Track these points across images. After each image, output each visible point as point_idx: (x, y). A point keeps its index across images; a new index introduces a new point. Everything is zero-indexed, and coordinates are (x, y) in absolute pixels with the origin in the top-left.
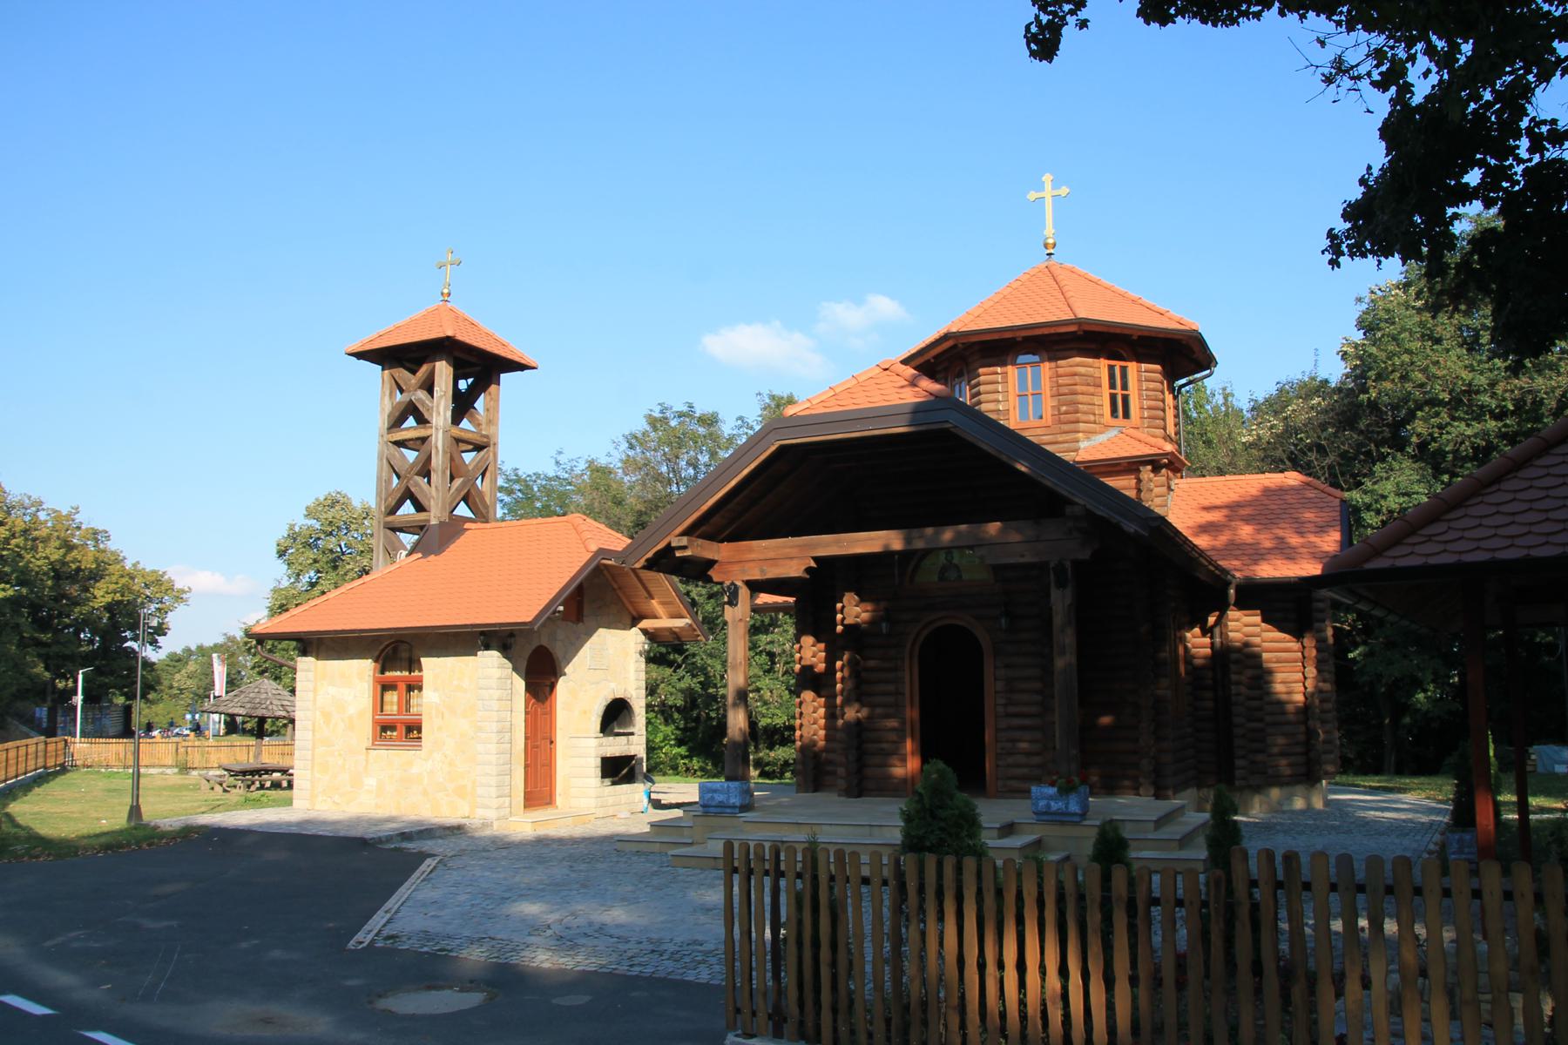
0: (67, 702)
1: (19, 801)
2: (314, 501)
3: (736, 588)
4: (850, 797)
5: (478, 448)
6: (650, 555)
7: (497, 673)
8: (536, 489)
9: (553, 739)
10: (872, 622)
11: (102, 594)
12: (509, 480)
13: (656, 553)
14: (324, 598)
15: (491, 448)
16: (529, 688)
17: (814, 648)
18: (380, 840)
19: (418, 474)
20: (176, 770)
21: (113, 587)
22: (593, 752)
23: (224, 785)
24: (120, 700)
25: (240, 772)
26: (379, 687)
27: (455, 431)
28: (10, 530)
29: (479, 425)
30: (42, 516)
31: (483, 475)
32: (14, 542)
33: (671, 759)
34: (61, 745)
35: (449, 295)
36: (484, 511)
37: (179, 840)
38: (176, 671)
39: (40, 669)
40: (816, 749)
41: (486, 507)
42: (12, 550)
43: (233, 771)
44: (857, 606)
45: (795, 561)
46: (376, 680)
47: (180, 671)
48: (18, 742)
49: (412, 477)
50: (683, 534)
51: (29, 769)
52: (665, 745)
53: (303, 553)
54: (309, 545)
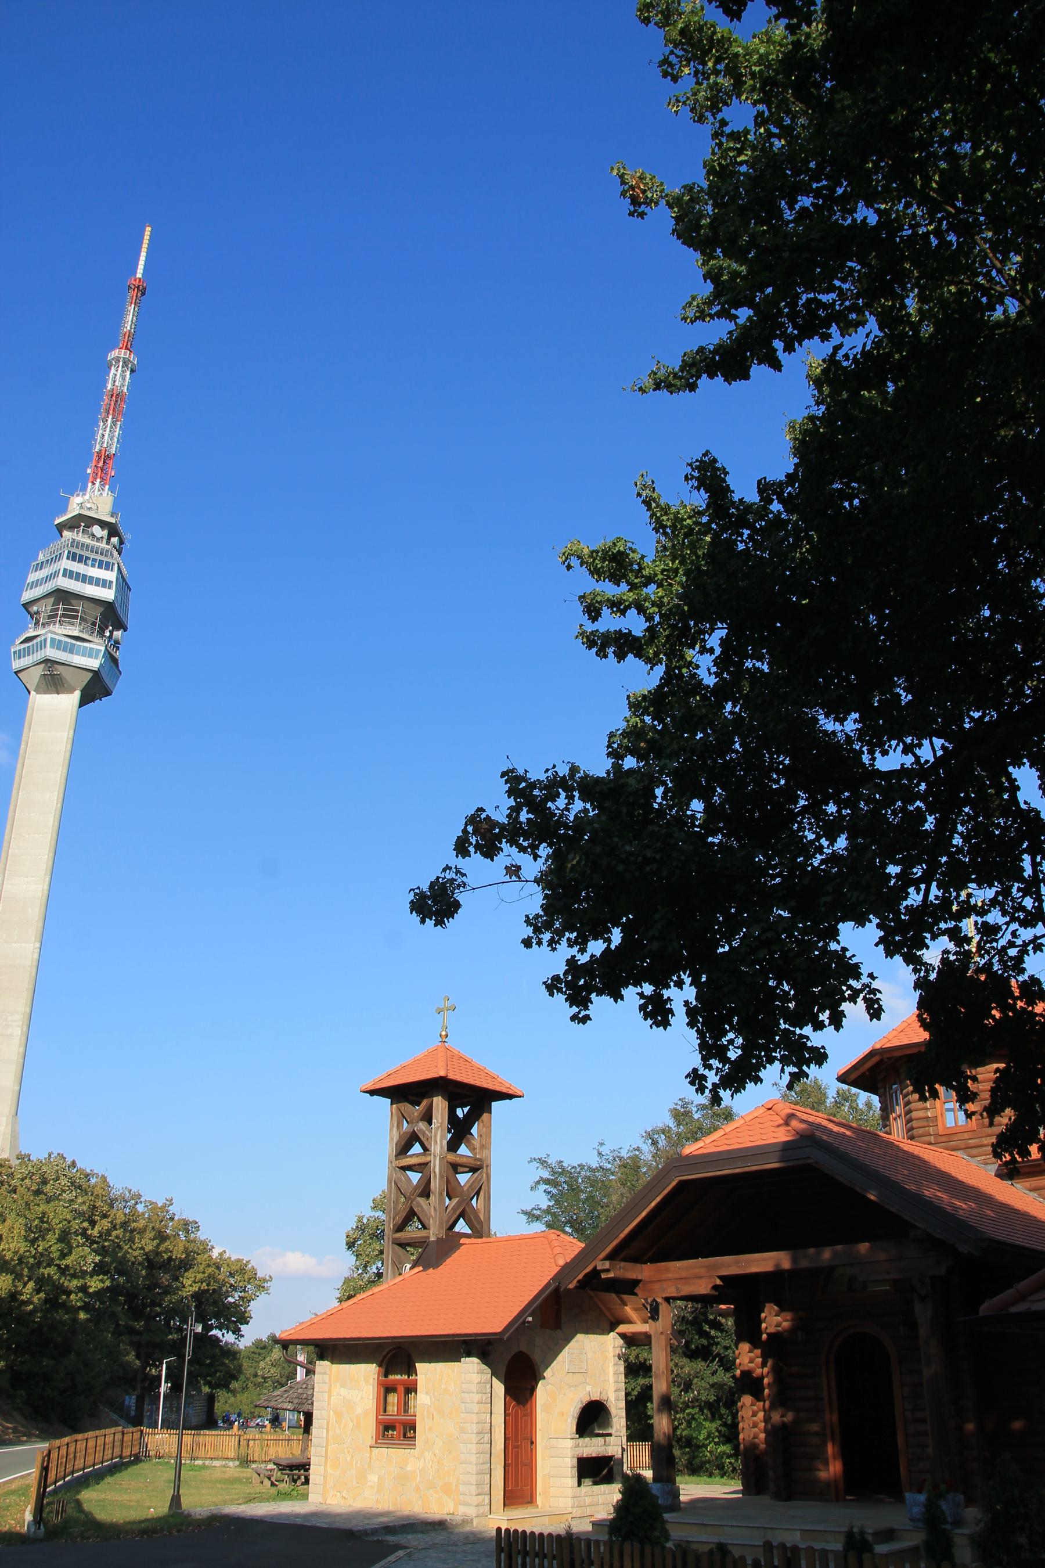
0: (154, 1391)
1: (91, 1488)
2: (381, 1193)
3: (657, 1304)
4: (779, 1500)
5: (474, 1170)
6: (580, 1277)
7: (476, 1378)
8: (580, 1180)
9: (534, 1440)
10: (792, 1331)
11: (190, 1284)
12: (554, 1173)
13: (586, 1275)
14: (351, 1302)
15: (485, 1170)
16: (508, 1392)
17: (752, 1355)
18: (365, 1533)
19: (421, 1195)
20: (237, 1463)
21: (200, 1276)
22: (569, 1453)
23: (273, 1479)
24: (206, 1389)
25: (287, 1466)
26: (382, 1390)
27: (451, 1157)
28: (112, 1222)
29: (474, 1149)
30: (140, 1208)
31: (478, 1193)
32: (114, 1233)
33: (717, 1458)
34: (137, 1436)
35: (447, 1036)
36: (478, 1227)
37: (203, 1527)
38: (261, 1358)
39: (131, 1357)
40: (758, 1452)
41: (481, 1223)
42: (113, 1241)
43: (281, 1465)
44: (776, 1316)
45: (703, 1280)
46: (380, 1384)
47: (264, 1358)
48: (97, 1431)
49: (415, 1198)
50: (606, 1259)
51: (106, 1458)
52: (710, 1443)
53: (370, 1244)
54: (377, 1237)
